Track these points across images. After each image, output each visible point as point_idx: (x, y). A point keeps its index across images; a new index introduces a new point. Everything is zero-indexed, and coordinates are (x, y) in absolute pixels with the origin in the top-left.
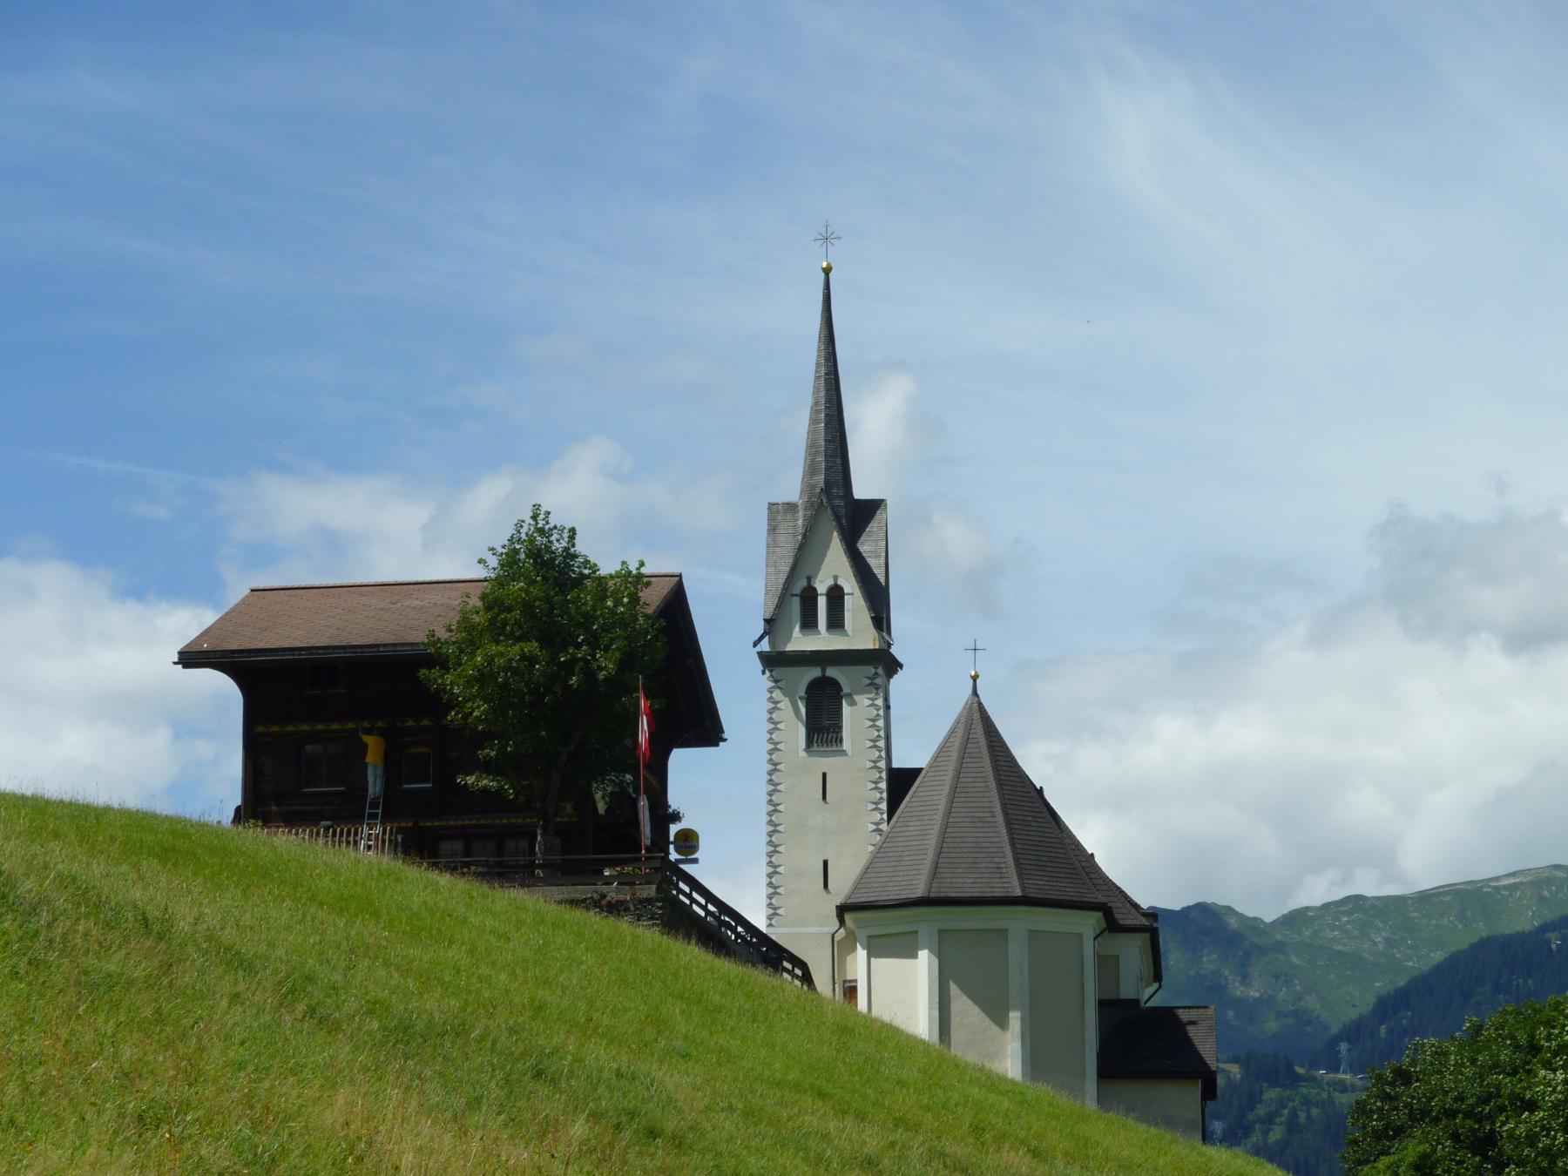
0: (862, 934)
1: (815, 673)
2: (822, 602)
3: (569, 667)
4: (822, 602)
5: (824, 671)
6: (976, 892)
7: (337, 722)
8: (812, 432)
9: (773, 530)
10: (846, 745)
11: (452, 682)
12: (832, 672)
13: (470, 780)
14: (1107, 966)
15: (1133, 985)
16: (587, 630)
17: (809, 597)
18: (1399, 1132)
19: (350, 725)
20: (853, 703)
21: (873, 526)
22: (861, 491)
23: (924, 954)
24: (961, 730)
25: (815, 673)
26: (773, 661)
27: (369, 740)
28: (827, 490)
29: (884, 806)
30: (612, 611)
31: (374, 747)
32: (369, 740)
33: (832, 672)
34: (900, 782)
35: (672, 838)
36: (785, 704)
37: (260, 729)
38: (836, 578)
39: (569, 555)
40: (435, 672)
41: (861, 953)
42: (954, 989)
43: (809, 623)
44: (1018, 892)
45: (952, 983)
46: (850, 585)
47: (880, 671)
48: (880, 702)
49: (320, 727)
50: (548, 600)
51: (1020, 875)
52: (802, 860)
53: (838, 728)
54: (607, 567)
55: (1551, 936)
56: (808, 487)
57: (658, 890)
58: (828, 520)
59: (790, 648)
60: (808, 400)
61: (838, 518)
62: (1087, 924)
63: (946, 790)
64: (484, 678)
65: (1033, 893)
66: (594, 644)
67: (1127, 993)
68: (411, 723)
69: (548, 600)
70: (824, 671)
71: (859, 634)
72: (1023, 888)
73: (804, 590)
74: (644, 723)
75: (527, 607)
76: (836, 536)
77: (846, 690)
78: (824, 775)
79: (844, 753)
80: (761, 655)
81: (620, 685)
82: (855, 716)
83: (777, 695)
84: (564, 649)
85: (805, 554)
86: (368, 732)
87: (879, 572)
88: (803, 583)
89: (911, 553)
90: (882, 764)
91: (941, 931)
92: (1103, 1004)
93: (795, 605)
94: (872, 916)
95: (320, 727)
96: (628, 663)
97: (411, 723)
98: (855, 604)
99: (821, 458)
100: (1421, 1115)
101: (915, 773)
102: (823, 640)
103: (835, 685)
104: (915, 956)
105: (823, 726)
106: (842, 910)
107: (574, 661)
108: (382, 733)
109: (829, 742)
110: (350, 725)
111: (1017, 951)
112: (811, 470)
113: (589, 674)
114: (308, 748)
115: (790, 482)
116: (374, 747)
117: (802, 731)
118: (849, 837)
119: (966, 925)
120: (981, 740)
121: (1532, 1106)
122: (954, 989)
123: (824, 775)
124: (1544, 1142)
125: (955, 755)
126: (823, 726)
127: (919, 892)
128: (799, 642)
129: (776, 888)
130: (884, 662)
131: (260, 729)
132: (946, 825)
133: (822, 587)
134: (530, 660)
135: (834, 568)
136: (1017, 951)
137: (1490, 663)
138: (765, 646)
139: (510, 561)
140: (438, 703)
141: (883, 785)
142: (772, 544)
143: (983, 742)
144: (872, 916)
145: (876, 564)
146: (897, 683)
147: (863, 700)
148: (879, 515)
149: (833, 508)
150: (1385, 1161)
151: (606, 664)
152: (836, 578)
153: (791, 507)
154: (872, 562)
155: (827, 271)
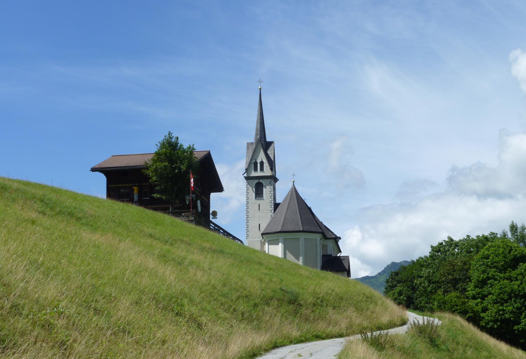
0: (267, 240)
1: (257, 181)
2: (259, 165)
3: (175, 168)
4: (259, 165)
6: (292, 230)
7: (123, 182)
8: (257, 126)
9: (248, 149)
10: (264, 197)
11: (149, 173)
13: (155, 195)
14: (324, 247)
15: (330, 251)
16: (180, 160)
17: (256, 164)
18: (396, 286)
19: (131, 185)
20: (266, 188)
21: (271, 147)
22: (268, 139)
23: (280, 244)
24: (290, 195)
25: (257, 181)
26: (248, 178)
27: (135, 188)
28: (260, 140)
29: (273, 211)
30: (186, 156)
31: (136, 189)
32: (135, 188)
34: (276, 206)
35: (211, 213)
36: (250, 188)
37: (110, 186)
39: (177, 143)
40: (145, 171)
41: (267, 244)
42: (287, 252)
43: (256, 170)
44: (302, 229)
46: (265, 161)
48: (272, 188)
49: (124, 185)
50: (170, 153)
51: (302, 226)
52: (254, 224)
53: (262, 193)
54: (185, 146)
56: (256, 139)
57: (194, 218)
58: (260, 146)
59: (251, 175)
60: (256, 119)
61: (262, 146)
62: (318, 237)
63: (286, 207)
64: (156, 170)
65: (305, 230)
66: (181, 163)
67: (329, 253)
68: (144, 184)
69: (170, 153)
71: (267, 172)
74: (192, 180)
75: (165, 154)
76: (262, 150)
77: (264, 185)
79: (264, 199)
80: (245, 177)
81: (187, 173)
82: (267, 191)
83: (248, 186)
84: (174, 164)
85: (255, 154)
86: (135, 186)
87: (272, 158)
88: (254, 161)
89: (279, 152)
90: (272, 202)
91: (284, 239)
92: (323, 256)
93: (253, 165)
94: (269, 236)
95: (124, 185)
96: (189, 167)
97: (144, 184)
98: (266, 165)
99: (259, 132)
100: (399, 282)
101: (279, 204)
102: (259, 174)
103: (262, 184)
104: (278, 244)
105: (259, 193)
106: (262, 234)
107: (176, 167)
108: (138, 186)
109: (260, 197)
110: (131, 185)
111: (302, 242)
112: (257, 135)
113: (180, 169)
114: (122, 190)
115: (252, 137)
116: (136, 189)
117: (254, 194)
118: (264, 217)
119: (293, 237)
120: (295, 195)
121: (421, 277)
122: (287, 252)
124: (423, 284)
125: (288, 199)
126: (259, 193)
127: (279, 230)
128: (253, 174)
130: (274, 179)
131: (110, 186)
132: (286, 215)
133: (259, 161)
134: (165, 166)
135: (261, 157)
136: (302, 242)
137: (473, 202)
139: (163, 145)
140: (147, 178)
141: (273, 207)
142: (248, 152)
143: (295, 196)
144: (269, 236)
145: (272, 156)
146: (277, 184)
147: (268, 187)
148: (272, 145)
149: (262, 144)
150: (392, 292)
151: (183, 168)
153: (252, 143)
154: (270, 155)
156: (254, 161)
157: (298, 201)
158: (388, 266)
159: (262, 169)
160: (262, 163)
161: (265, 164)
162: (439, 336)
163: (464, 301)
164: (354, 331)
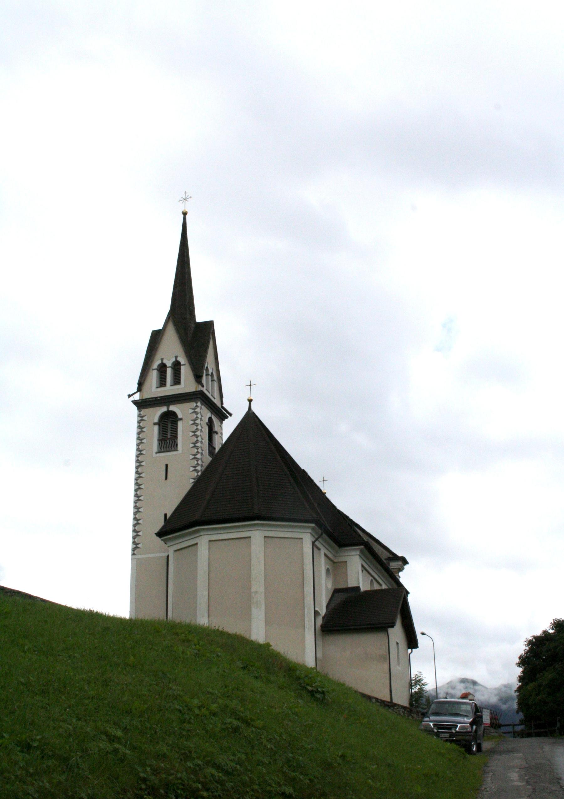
1: (164, 409)
2: (169, 372)
4: (169, 372)
5: (168, 408)
12: (173, 408)
22: (200, 317)
25: (164, 409)
33: (173, 408)
38: (176, 357)
45: (217, 450)
47: (199, 404)
51: (267, 622)
53: (175, 436)
55: (459, 725)
70: (168, 408)
72: (266, 637)
73: (159, 365)
78: (167, 466)
80: (135, 403)
98: (186, 372)
102: (169, 389)
103: (174, 414)
122: (391, 556)
123: (167, 466)
129: (138, 508)
138: (137, 397)
152: (176, 357)
155: (185, 214)
156: (156, 364)
157: (403, 605)
158: (324, 494)
159: (177, 380)
160: (177, 366)
161: (183, 368)
162: (155, 784)
163: (236, 767)
164: (96, 709)
